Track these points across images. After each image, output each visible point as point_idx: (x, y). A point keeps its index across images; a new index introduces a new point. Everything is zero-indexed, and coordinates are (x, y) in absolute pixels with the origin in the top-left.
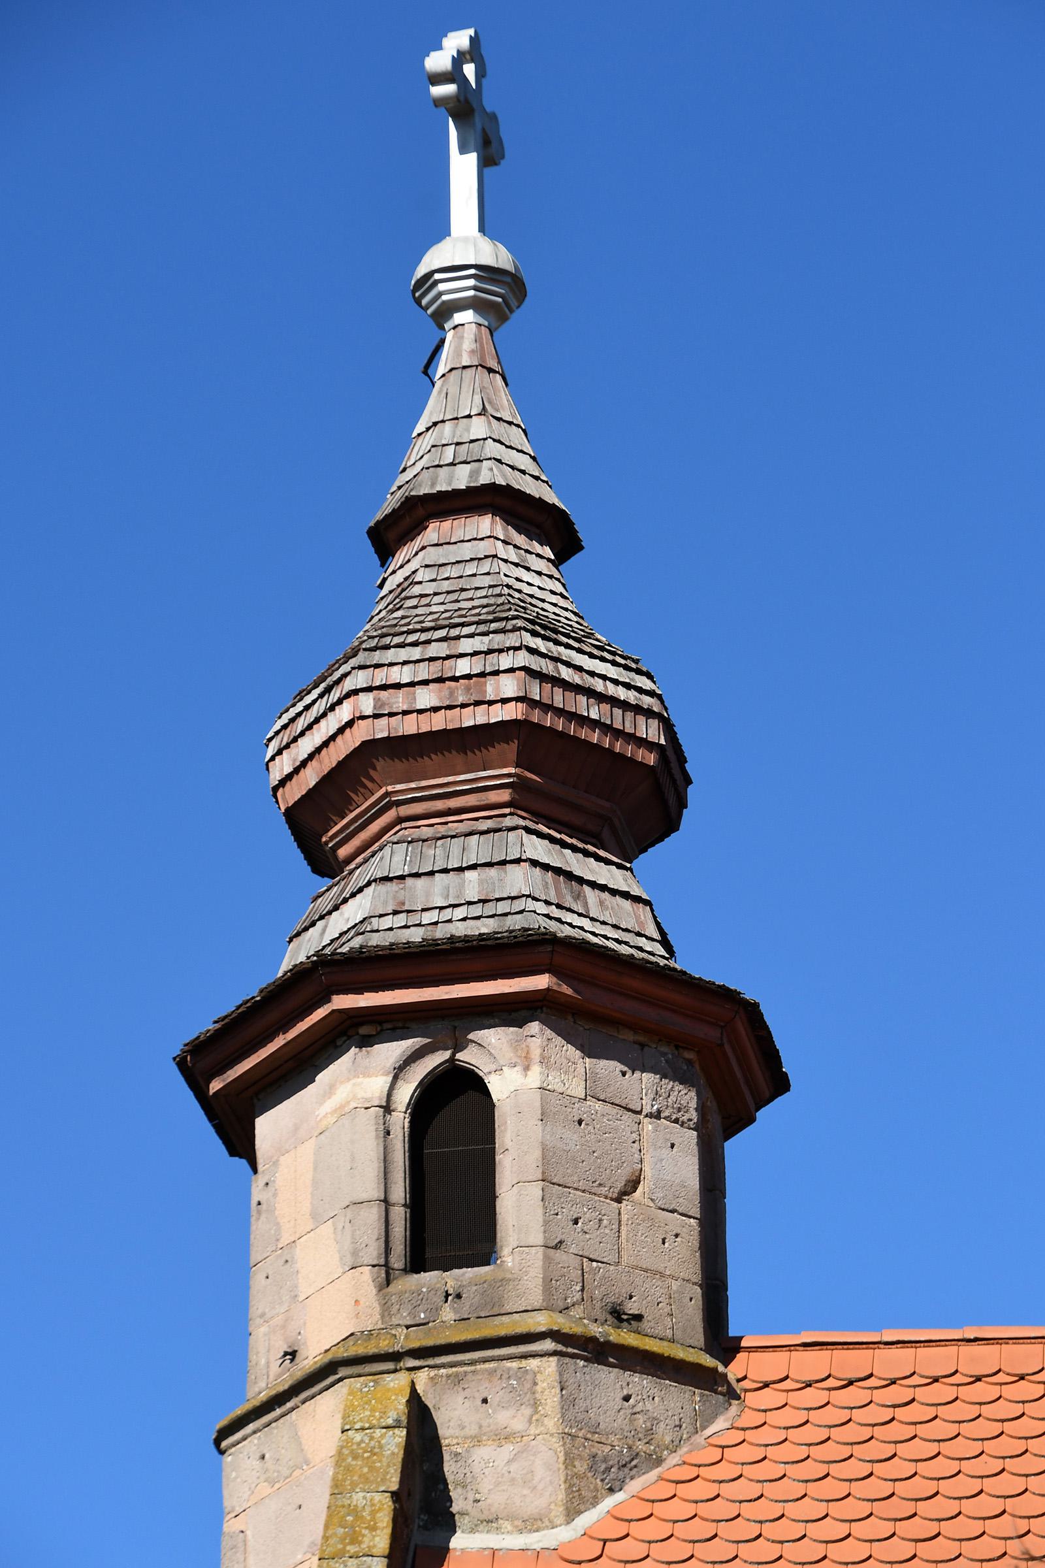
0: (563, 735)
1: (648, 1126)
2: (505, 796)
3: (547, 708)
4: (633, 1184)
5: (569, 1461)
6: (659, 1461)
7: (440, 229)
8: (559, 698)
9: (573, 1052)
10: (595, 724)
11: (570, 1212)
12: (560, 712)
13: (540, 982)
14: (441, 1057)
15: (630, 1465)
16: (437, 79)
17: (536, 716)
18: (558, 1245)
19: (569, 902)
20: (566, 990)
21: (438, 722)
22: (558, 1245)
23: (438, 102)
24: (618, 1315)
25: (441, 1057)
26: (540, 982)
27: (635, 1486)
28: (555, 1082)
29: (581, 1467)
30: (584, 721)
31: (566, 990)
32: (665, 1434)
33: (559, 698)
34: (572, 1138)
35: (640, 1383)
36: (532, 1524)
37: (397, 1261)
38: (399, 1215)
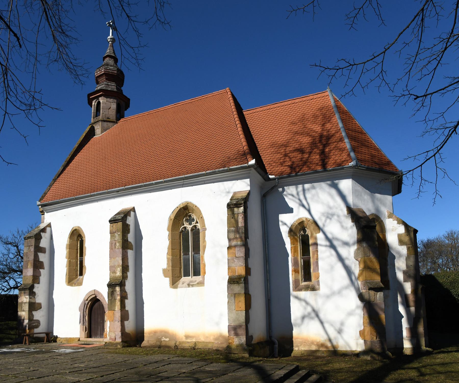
0: (108, 73)
1: (112, 103)
2: (105, 79)
3: (106, 71)
4: (110, 108)
5: (101, 130)
6: (109, 129)
7: (109, 35)
8: (107, 70)
9: (105, 98)
10: (111, 72)
11: (104, 111)
12: (107, 72)
13: (101, 93)
14: (98, 101)
15: (107, 129)
16: (107, 24)
17: (105, 72)
18: (103, 114)
19: (108, 87)
20: (103, 93)
21: (100, 74)
22: (103, 114)
23: (108, 26)
24: (108, 118)
25: (98, 101)
26: (101, 93)
27: (107, 131)
28: (104, 101)
29: (102, 130)
30: (110, 72)
31: (103, 93)
32: (110, 127)
33: (107, 70)
34: (105, 105)
35: (108, 123)
36: (99, 135)
37: (95, 117)
38: (95, 113)
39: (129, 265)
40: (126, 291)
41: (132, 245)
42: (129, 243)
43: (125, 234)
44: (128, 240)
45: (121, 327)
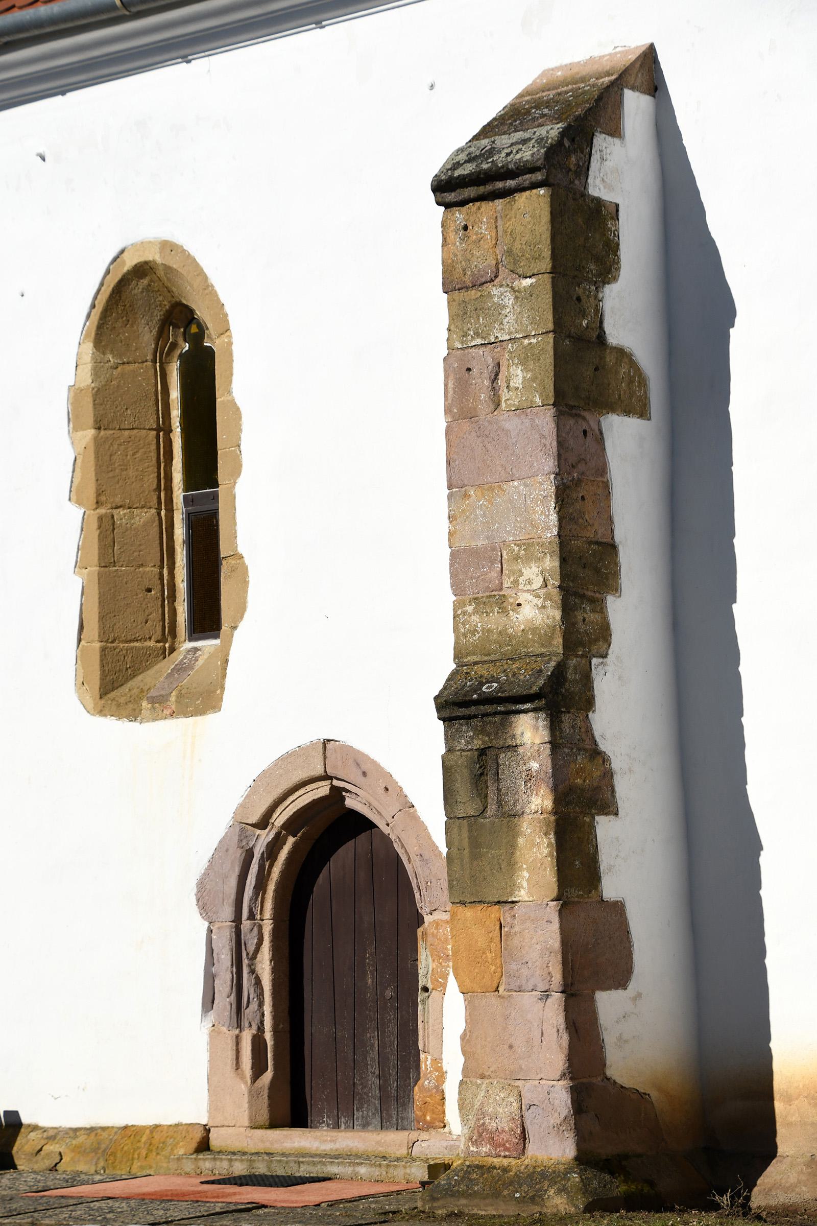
39: (619, 536)
40: (603, 746)
41: (637, 377)
42: (610, 359)
43: (579, 291)
44: (601, 337)
45: (565, 1038)
